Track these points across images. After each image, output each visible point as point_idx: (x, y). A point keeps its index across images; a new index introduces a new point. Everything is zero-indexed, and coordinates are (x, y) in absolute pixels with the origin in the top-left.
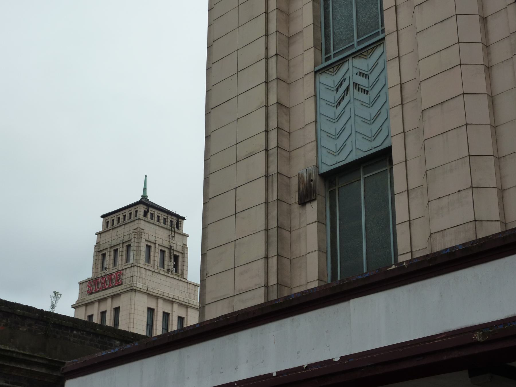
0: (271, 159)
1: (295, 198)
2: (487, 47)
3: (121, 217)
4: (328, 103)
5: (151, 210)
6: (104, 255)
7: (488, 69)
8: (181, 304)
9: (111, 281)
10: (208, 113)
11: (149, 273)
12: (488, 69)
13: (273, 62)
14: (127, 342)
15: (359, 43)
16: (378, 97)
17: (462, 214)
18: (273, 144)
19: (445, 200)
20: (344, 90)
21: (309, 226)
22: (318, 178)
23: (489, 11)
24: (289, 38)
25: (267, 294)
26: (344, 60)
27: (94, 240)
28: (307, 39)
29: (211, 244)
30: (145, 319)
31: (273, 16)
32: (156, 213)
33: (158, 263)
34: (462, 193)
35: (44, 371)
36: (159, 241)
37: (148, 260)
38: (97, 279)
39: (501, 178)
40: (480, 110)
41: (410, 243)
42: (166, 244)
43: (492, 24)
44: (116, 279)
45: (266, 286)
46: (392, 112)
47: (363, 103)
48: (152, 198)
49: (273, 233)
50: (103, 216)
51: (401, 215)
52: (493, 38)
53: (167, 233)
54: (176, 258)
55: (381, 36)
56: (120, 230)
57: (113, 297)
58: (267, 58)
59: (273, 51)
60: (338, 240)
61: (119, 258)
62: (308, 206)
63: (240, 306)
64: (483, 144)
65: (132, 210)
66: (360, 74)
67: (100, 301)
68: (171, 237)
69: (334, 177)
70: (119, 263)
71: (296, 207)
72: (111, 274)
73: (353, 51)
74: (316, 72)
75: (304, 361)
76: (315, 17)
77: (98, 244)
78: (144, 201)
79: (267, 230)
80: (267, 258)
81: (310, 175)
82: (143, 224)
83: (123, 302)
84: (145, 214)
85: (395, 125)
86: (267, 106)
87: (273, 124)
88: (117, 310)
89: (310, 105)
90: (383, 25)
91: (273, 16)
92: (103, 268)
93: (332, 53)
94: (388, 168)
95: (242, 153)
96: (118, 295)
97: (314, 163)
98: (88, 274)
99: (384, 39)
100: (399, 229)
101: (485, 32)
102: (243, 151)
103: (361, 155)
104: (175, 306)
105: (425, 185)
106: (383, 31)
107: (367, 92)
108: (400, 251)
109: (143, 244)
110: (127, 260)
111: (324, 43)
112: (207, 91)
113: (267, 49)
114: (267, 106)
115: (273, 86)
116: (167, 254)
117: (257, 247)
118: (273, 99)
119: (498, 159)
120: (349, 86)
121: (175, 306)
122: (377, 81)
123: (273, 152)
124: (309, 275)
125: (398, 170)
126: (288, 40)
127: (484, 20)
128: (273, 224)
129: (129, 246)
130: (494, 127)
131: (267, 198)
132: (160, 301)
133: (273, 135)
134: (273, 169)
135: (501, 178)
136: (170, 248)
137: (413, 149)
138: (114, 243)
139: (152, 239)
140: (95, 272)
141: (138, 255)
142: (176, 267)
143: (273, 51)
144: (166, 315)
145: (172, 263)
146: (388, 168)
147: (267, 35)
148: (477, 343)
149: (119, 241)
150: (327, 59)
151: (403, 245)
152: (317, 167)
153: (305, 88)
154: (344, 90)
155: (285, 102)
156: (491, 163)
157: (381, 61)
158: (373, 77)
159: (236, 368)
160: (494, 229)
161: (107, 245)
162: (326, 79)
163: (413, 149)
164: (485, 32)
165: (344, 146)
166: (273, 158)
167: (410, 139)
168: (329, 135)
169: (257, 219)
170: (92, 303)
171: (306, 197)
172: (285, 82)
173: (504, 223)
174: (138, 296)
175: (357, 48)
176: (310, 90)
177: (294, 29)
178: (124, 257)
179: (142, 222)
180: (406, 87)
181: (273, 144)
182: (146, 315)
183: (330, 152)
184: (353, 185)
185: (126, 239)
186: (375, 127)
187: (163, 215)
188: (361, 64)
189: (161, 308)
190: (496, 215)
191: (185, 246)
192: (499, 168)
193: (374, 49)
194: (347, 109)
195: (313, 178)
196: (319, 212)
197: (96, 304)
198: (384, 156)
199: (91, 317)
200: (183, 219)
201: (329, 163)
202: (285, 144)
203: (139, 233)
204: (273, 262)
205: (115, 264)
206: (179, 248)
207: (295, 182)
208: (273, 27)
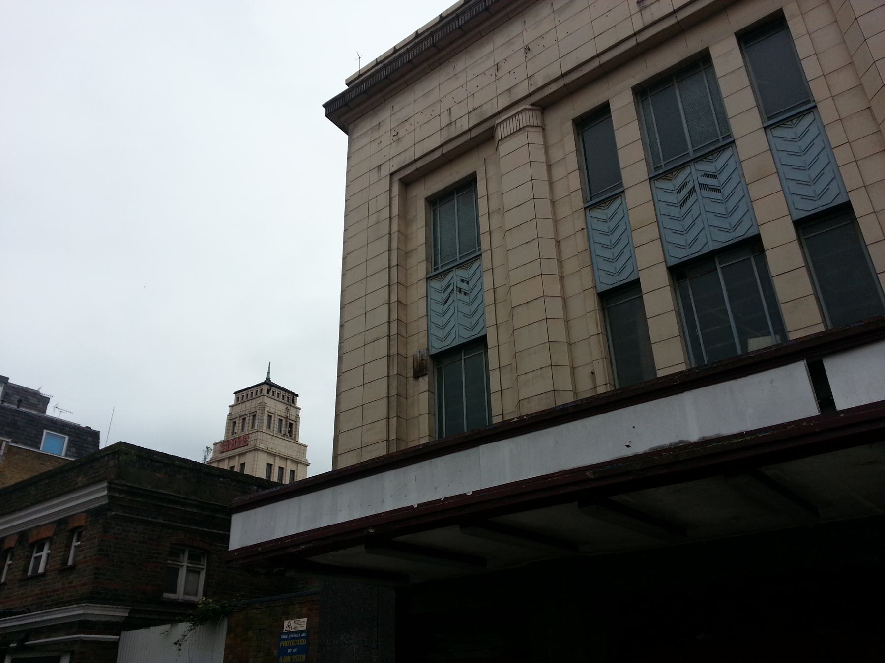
0: (392, 343)
2: (560, 262)
3: (254, 392)
4: (437, 302)
5: (273, 389)
6: (234, 423)
7: (562, 278)
8: (293, 461)
10: (342, 308)
11: (270, 437)
12: (562, 278)
13: (394, 270)
14: (264, 488)
15: (442, 267)
16: (476, 298)
17: (543, 385)
18: (394, 331)
19: (530, 375)
20: (449, 293)
21: (421, 396)
22: (429, 358)
23: (562, 236)
24: (407, 253)
25: (388, 447)
26: (449, 270)
27: (227, 411)
28: (421, 254)
29: (343, 407)
31: (395, 237)
32: (277, 391)
33: (276, 429)
34: (544, 370)
35: (195, 510)
36: (278, 413)
37: (269, 427)
39: (572, 360)
40: (555, 308)
41: (502, 408)
42: (283, 414)
43: (564, 245)
45: (388, 440)
46: (487, 309)
47: (464, 303)
48: (274, 380)
49: (394, 399)
50: (235, 393)
51: (494, 386)
52: (565, 256)
53: (285, 406)
54: (291, 425)
56: (248, 404)
57: (240, 455)
58: (390, 267)
60: (445, 407)
61: (246, 425)
62: (421, 379)
63: (367, 457)
64: (559, 333)
65: (259, 389)
66: (462, 281)
67: (230, 458)
68: (287, 409)
69: (440, 358)
70: (246, 428)
71: (411, 380)
73: (718, 145)
74: (650, 179)
75: (441, 495)
78: (268, 382)
79: (388, 397)
80: (388, 418)
81: (422, 356)
82: (266, 399)
83: (248, 459)
84: (268, 391)
85: (490, 319)
86: (389, 303)
87: (394, 316)
89: (423, 303)
90: (479, 244)
91: (395, 237)
92: (233, 433)
93: (440, 265)
94: (483, 351)
95: (369, 338)
96: (244, 454)
97: (426, 347)
98: (221, 436)
99: (623, 191)
100: (493, 397)
101: (559, 252)
102: (370, 336)
103: (463, 341)
104: (289, 462)
105: (514, 364)
106: (480, 249)
107: (468, 294)
108: (494, 414)
109: (266, 415)
110: (253, 426)
111: (433, 258)
112: (342, 291)
113: (390, 260)
114: (389, 303)
115: (394, 288)
116: (284, 423)
117: (381, 410)
118: (394, 298)
119: (570, 344)
120: (694, 187)
121: (289, 462)
122: (475, 286)
123: (394, 338)
124: (421, 432)
125: (492, 354)
126: (405, 254)
127: (558, 243)
128: (394, 392)
129: (254, 416)
130: (567, 322)
131: (389, 373)
132: (277, 458)
133: (394, 325)
134: (394, 351)
135: (572, 360)
136: (287, 418)
137: (504, 337)
138: (243, 413)
139: (273, 411)
140: (226, 436)
141: (262, 422)
142: (290, 432)
143: (394, 262)
144: (281, 469)
145: (288, 429)
146: (483, 351)
147: (390, 250)
148: (590, 480)
150: (436, 270)
151: (496, 408)
152: (428, 350)
153: (418, 291)
154: (449, 293)
155: (403, 300)
156: (565, 347)
157: (478, 272)
158: (472, 283)
159: (383, 502)
160: (568, 398)
161: (237, 415)
162: (435, 284)
163: (504, 337)
164: (559, 252)
165: (449, 334)
166: (394, 343)
167: (502, 329)
168: (438, 326)
169: (381, 388)
170: (223, 460)
172: (403, 285)
173: (576, 393)
175: (459, 262)
176: (423, 291)
177: (412, 246)
180: (498, 291)
181: (394, 331)
182: (265, 469)
183: (438, 338)
184: (456, 365)
185: (253, 410)
186: (474, 321)
188: (462, 273)
189: (278, 463)
190: (569, 387)
191: (298, 417)
192: (570, 352)
193: (473, 263)
194: (452, 307)
195: (425, 358)
196: (430, 384)
197: (237, 458)
198: (482, 341)
199: (233, 467)
200: (297, 396)
201: (438, 347)
202: (403, 333)
203: (263, 406)
204: (394, 421)
205: (243, 430)
206: (293, 418)
208: (395, 244)
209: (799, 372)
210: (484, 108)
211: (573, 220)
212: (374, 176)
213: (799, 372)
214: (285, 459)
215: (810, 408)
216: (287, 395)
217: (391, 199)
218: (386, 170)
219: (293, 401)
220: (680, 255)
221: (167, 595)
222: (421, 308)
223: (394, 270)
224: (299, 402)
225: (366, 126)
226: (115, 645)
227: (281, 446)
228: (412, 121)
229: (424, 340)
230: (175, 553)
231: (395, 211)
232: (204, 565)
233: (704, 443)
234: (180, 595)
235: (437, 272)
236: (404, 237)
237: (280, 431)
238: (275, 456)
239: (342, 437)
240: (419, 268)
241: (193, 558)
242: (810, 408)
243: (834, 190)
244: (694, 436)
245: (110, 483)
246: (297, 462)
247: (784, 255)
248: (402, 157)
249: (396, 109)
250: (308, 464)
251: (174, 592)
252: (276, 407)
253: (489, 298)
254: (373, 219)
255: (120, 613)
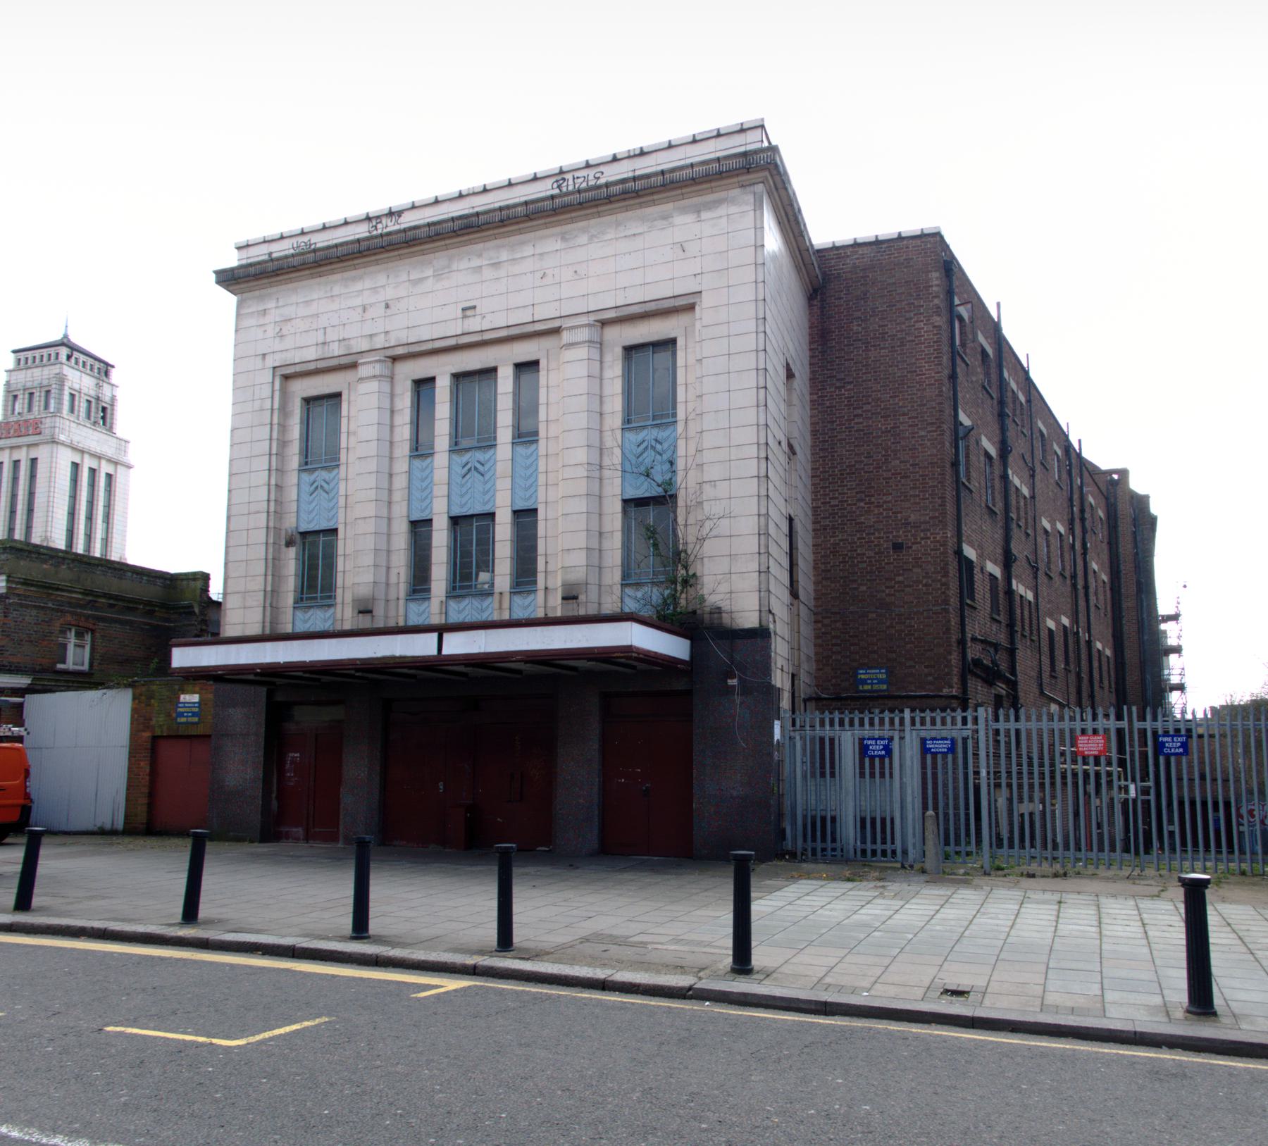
1: (283, 542)
5: (76, 354)
6: (15, 397)
8: (110, 461)
9: (27, 428)
11: (74, 425)
13: (274, 458)
18: (272, 509)
20: (468, 471)
26: (316, 469)
30: (69, 474)
31: (275, 427)
32: (82, 358)
37: (72, 410)
38: (7, 423)
39: (388, 561)
42: (93, 393)
44: (33, 428)
48: (76, 339)
49: (270, 561)
54: (104, 409)
55: (671, 420)
59: (274, 451)
61: (36, 404)
68: (98, 386)
70: (35, 409)
71: (283, 548)
72: (26, 421)
76: (301, 435)
77: (8, 384)
82: (67, 370)
83: (42, 453)
84: (69, 357)
85: (341, 519)
87: (273, 497)
88: (34, 461)
91: (275, 427)
101: (391, 452)
102: (254, 508)
110: (47, 406)
111: (306, 452)
115: (274, 473)
116: (93, 405)
118: (273, 482)
126: (283, 444)
128: (270, 556)
129: (48, 392)
133: (272, 504)
136: (98, 399)
138: (29, 385)
139: (77, 387)
142: (104, 418)
144: (93, 471)
149: (36, 384)
153: (292, 479)
154: (468, 471)
166: (272, 518)
171: (289, 544)
172: (281, 471)
174: (61, 449)
178: (43, 403)
179: (65, 367)
181: (272, 509)
184: (315, 553)
185: (45, 382)
187: (90, 361)
189: (88, 463)
191: (113, 398)
196: (297, 554)
201: (304, 527)
203: (61, 380)
204: (270, 578)
205: (30, 409)
206: (107, 399)
207: (283, 533)
209: (435, 636)
210: (352, 342)
211: (402, 466)
212: (258, 363)
213: (435, 636)
214: (99, 457)
215: (435, 652)
216: (97, 365)
217: (273, 391)
218: (270, 362)
219: (107, 374)
220: (457, 511)
221: (60, 666)
222: (293, 494)
223: (274, 458)
224: (115, 376)
225: (254, 307)
226: (21, 705)
227: (92, 438)
228: (294, 322)
229: (294, 520)
230: (63, 632)
231: (276, 406)
232: (88, 637)
233: (401, 657)
234: (70, 665)
235: (307, 463)
236: (283, 427)
237: (89, 417)
238: (83, 452)
239: (230, 581)
240: (294, 462)
241: (79, 635)
242: (433, 651)
243: (533, 500)
244: (398, 654)
245: (9, 576)
246: (116, 463)
247: (503, 530)
248: (284, 355)
249: (281, 304)
250: (129, 467)
251: (64, 662)
252: (79, 380)
253: (342, 502)
254: (257, 404)
255: (23, 681)
